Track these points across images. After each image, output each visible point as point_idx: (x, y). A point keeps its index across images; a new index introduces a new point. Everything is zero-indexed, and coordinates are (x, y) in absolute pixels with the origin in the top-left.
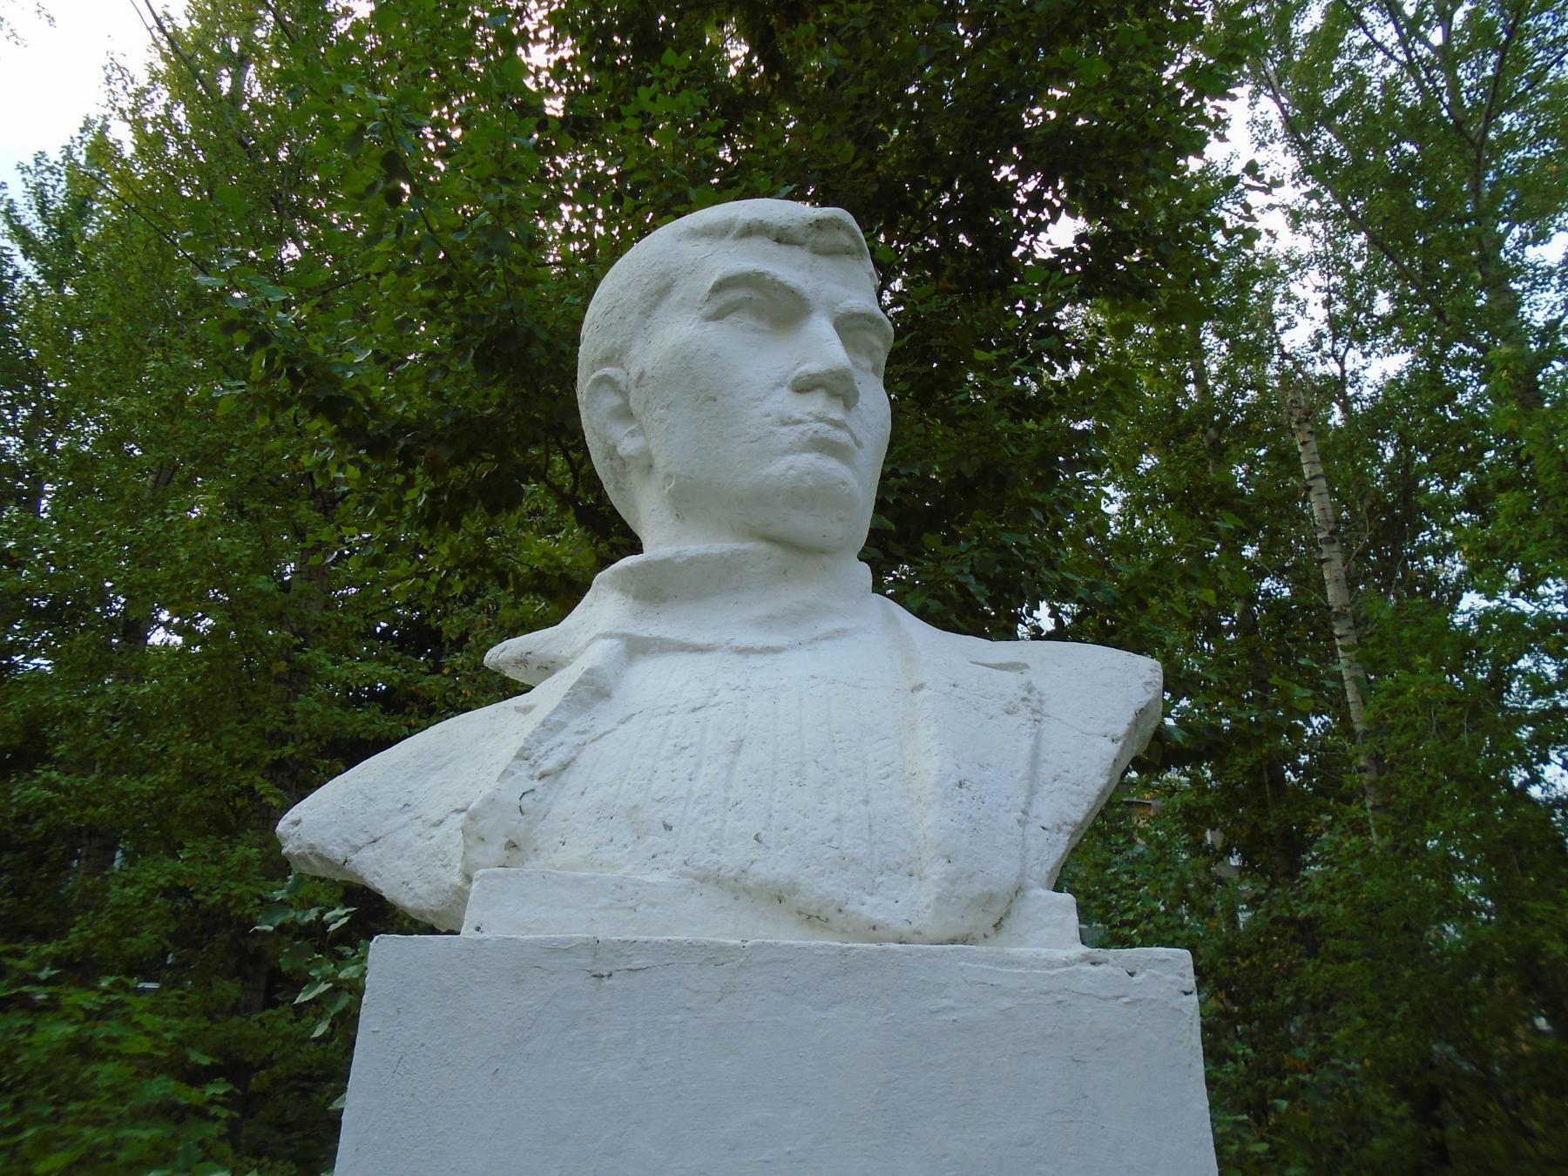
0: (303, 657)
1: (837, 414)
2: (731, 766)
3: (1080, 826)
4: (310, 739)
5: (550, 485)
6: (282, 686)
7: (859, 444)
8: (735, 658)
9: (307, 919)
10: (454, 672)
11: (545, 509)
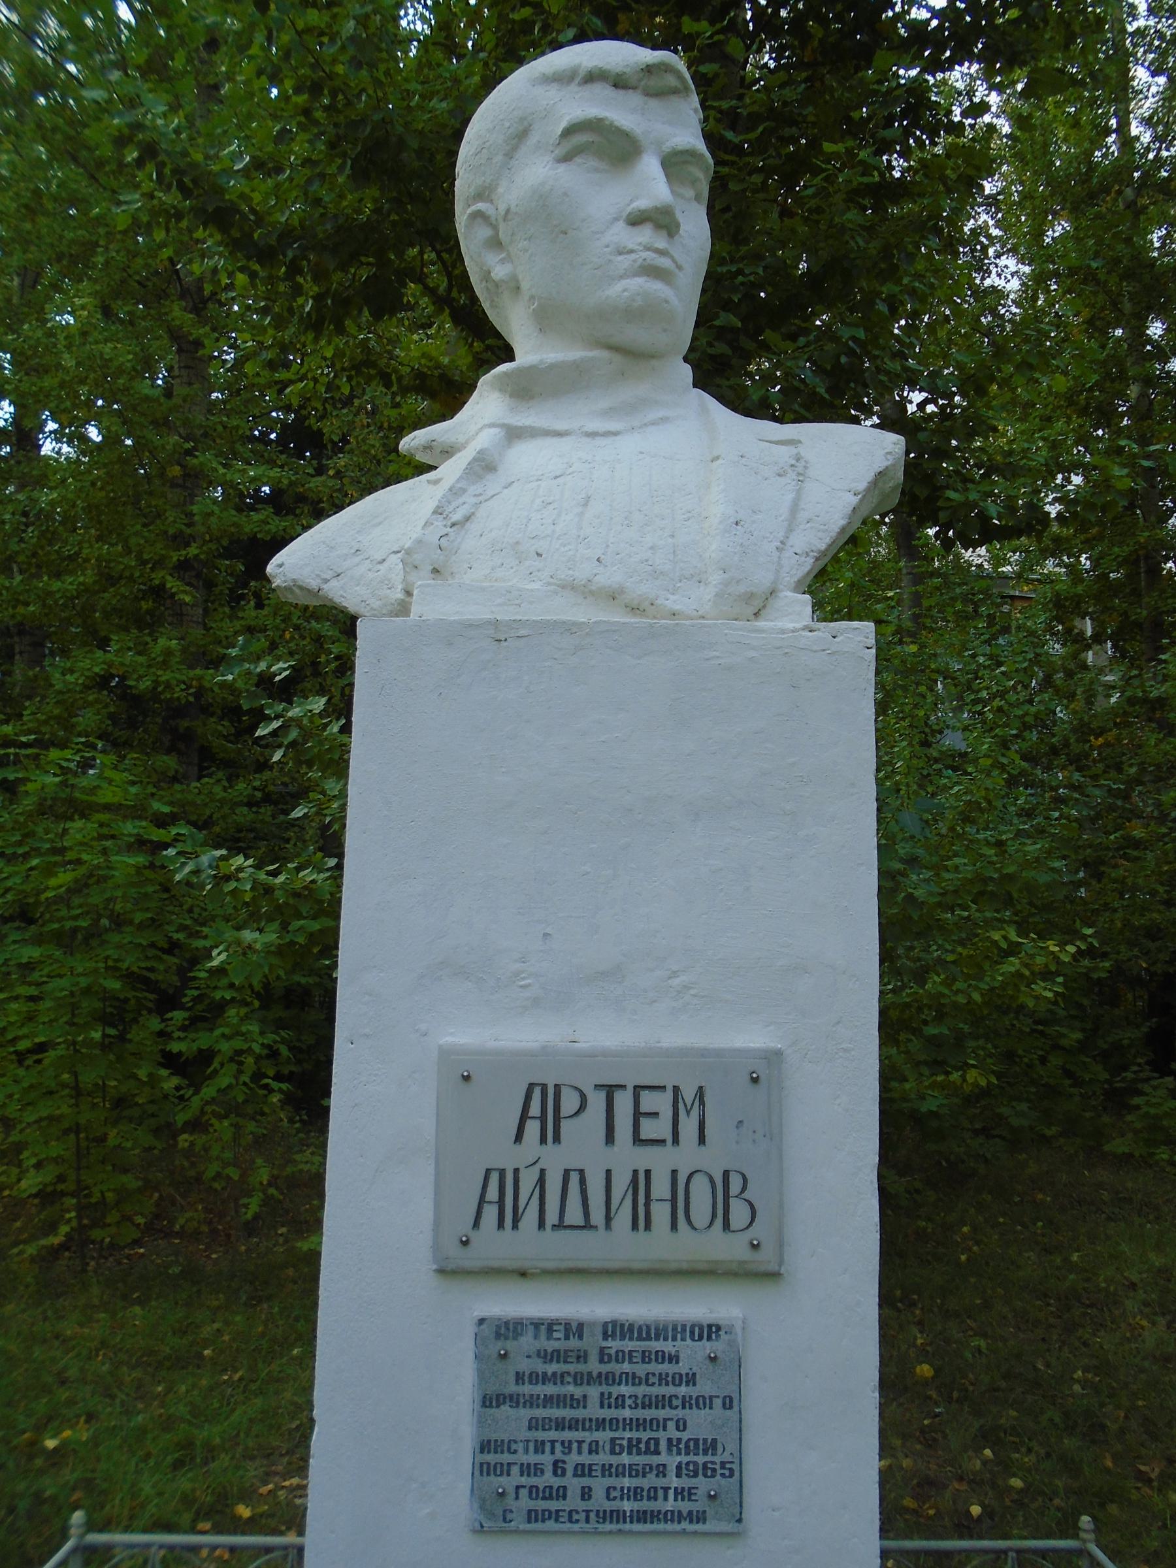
0: (195, 461)
1: (661, 244)
2: (581, 515)
3: (823, 553)
4: (211, 541)
5: (426, 287)
6: (178, 490)
7: (680, 268)
8: (588, 440)
9: (258, 670)
10: (339, 474)
11: (417, 303)
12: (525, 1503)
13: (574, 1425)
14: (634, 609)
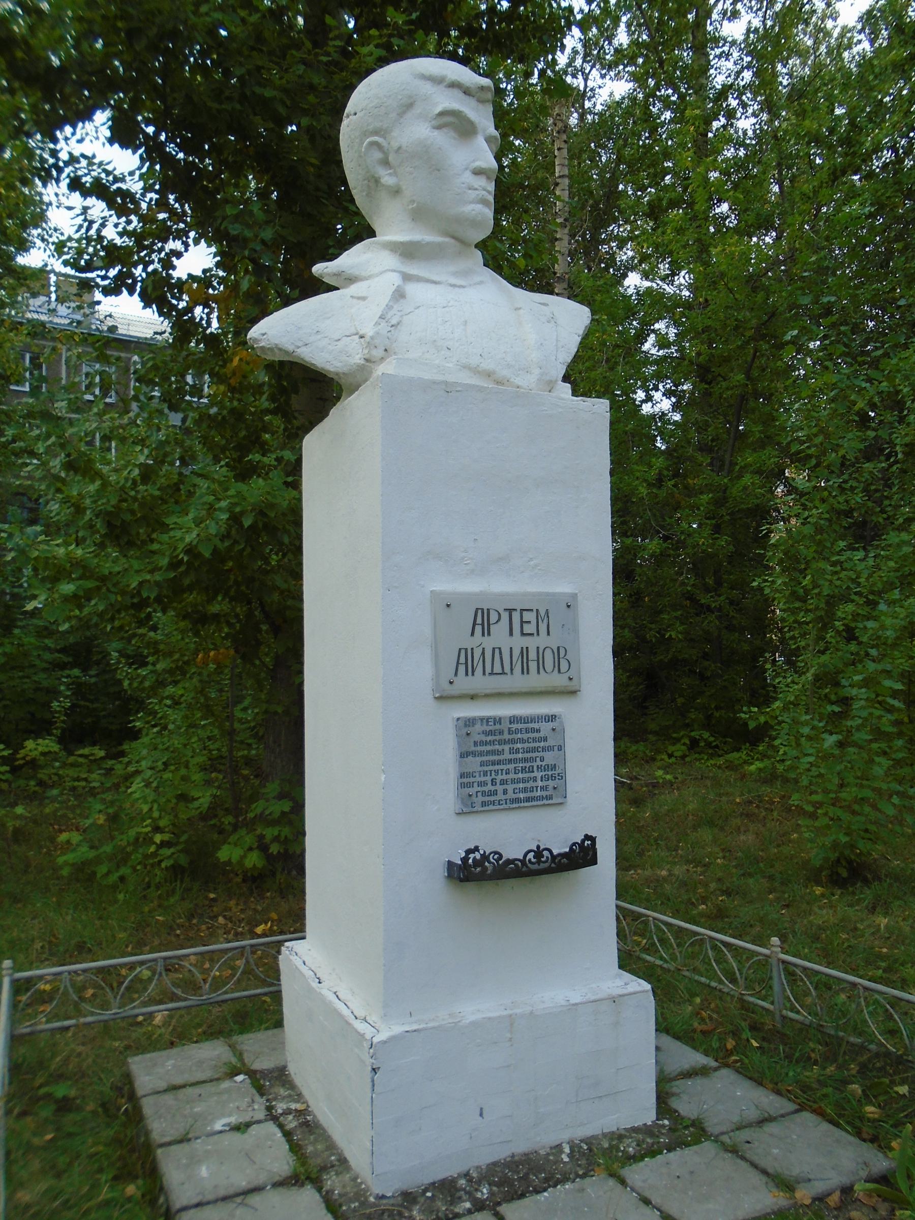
12: (481, 798)
13: (499, 763)
14: (498, 383)
